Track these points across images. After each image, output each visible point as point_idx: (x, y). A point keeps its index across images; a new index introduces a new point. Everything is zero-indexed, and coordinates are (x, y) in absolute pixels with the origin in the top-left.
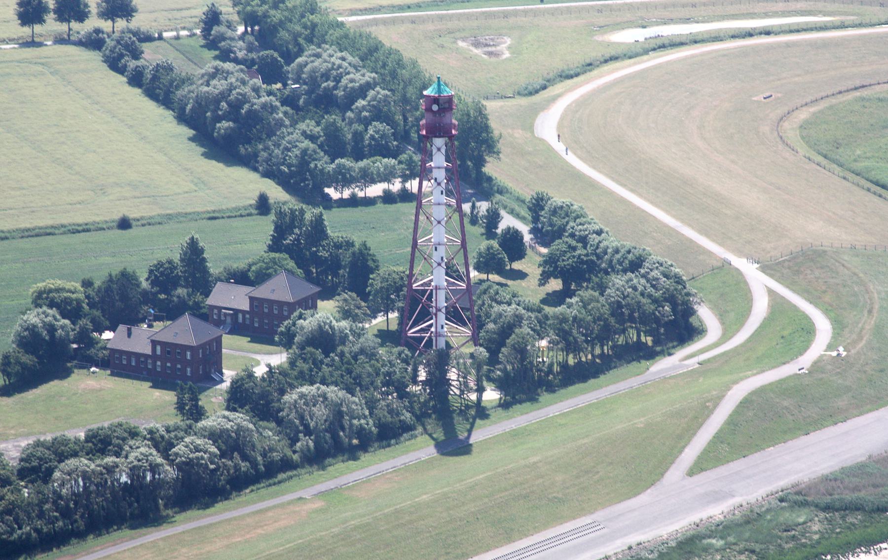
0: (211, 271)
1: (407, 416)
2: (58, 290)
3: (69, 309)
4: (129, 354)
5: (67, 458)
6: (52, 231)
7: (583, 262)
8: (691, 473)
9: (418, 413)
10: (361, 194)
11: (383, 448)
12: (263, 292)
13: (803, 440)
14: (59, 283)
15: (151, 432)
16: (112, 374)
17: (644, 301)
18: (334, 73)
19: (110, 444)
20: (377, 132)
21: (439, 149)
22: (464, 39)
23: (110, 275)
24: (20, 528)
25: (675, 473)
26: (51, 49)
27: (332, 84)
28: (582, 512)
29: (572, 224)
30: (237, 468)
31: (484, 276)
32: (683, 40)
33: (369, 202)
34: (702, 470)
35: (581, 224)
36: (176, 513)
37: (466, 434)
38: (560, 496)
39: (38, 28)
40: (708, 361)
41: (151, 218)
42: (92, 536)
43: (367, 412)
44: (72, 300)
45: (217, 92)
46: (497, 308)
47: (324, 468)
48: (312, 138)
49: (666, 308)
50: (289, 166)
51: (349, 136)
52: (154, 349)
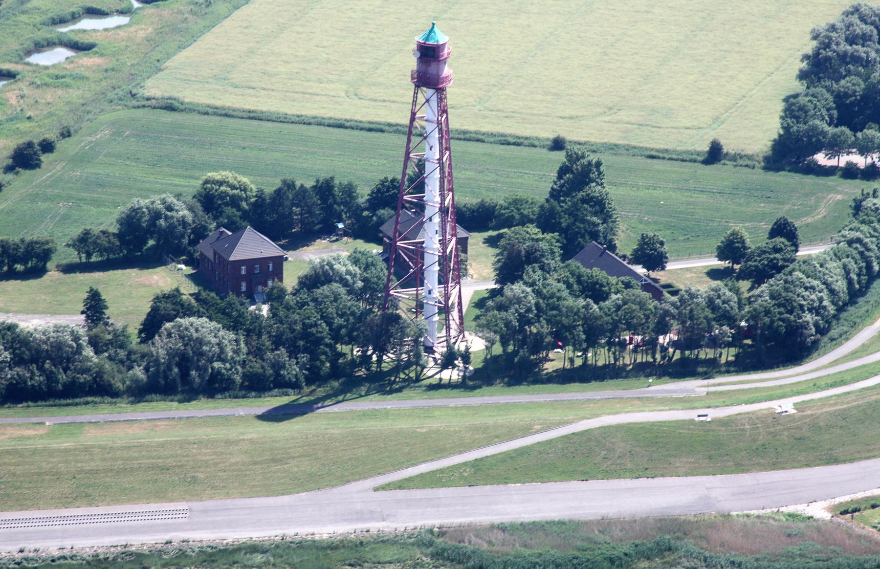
2: (221, 183)
38: (201, 476)
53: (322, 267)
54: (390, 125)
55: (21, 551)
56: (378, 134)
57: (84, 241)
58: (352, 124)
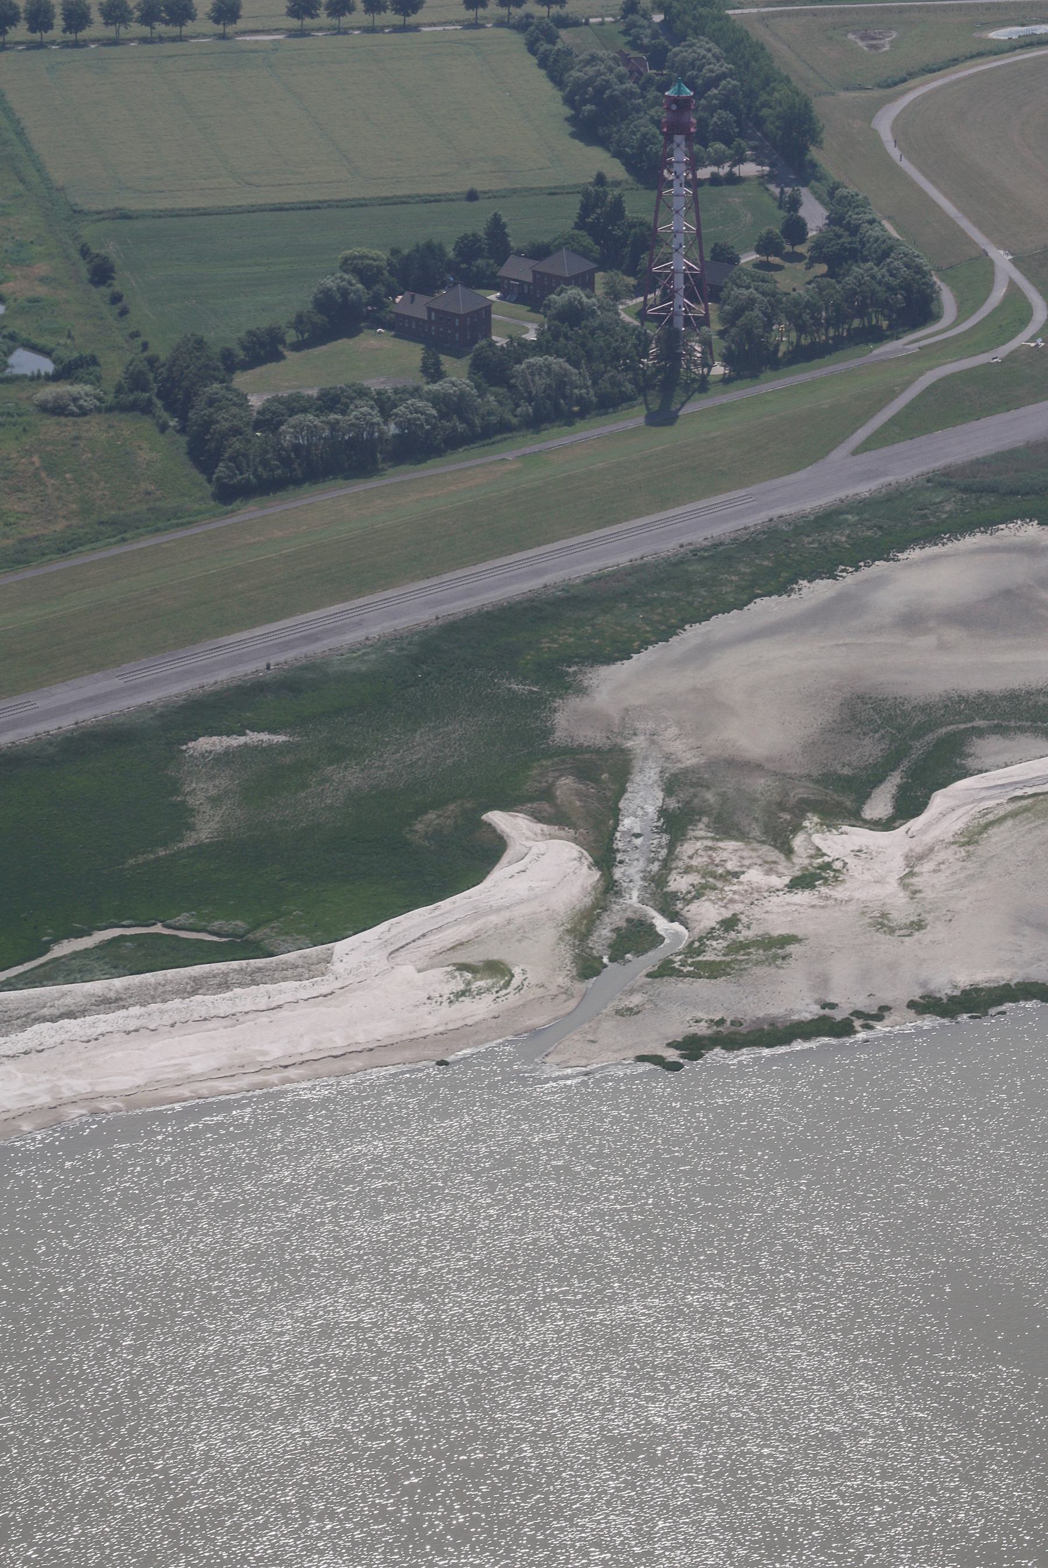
1: (629, 387)
2: (363, 257)
3: (367, 274)
4: (410, 318)
5: (296, 414)
6: (408, 200)
7: (846, 249)
8: (855, 453)
9: (642, 384)
11: (601, 415)
12: (545, 266)
14: (364, 250)
15: (379, 393)
16: (395, 336)
17: (878, 288)
18: (698, 63)
19: (338, 402)
20: (720, 119)
21: (678, 145)
22: (854, 32)
23: (417, 245)
24: (241, 474)
25: (839, 454)
26: (490, 31)
27: (695, 73)
29: (850, 213)
31: (764, 258)
34: (866, 450)
35: (857, 214)
36: (390, 467)
37: (678, 406)
39: (481, 12)
40: (925, 347)
41: (497, 191)
42: (307, 484)
43: (589, 383)
45: (586, 77)
46: (736, 291)
47: (538, 432)
48: (657, 123)
49: (899, 296)
50: (633, 148)
52: (429, 316)
54: (320, 202)
55: (681, 546)
56: (318, 211)
57: (299, 322)
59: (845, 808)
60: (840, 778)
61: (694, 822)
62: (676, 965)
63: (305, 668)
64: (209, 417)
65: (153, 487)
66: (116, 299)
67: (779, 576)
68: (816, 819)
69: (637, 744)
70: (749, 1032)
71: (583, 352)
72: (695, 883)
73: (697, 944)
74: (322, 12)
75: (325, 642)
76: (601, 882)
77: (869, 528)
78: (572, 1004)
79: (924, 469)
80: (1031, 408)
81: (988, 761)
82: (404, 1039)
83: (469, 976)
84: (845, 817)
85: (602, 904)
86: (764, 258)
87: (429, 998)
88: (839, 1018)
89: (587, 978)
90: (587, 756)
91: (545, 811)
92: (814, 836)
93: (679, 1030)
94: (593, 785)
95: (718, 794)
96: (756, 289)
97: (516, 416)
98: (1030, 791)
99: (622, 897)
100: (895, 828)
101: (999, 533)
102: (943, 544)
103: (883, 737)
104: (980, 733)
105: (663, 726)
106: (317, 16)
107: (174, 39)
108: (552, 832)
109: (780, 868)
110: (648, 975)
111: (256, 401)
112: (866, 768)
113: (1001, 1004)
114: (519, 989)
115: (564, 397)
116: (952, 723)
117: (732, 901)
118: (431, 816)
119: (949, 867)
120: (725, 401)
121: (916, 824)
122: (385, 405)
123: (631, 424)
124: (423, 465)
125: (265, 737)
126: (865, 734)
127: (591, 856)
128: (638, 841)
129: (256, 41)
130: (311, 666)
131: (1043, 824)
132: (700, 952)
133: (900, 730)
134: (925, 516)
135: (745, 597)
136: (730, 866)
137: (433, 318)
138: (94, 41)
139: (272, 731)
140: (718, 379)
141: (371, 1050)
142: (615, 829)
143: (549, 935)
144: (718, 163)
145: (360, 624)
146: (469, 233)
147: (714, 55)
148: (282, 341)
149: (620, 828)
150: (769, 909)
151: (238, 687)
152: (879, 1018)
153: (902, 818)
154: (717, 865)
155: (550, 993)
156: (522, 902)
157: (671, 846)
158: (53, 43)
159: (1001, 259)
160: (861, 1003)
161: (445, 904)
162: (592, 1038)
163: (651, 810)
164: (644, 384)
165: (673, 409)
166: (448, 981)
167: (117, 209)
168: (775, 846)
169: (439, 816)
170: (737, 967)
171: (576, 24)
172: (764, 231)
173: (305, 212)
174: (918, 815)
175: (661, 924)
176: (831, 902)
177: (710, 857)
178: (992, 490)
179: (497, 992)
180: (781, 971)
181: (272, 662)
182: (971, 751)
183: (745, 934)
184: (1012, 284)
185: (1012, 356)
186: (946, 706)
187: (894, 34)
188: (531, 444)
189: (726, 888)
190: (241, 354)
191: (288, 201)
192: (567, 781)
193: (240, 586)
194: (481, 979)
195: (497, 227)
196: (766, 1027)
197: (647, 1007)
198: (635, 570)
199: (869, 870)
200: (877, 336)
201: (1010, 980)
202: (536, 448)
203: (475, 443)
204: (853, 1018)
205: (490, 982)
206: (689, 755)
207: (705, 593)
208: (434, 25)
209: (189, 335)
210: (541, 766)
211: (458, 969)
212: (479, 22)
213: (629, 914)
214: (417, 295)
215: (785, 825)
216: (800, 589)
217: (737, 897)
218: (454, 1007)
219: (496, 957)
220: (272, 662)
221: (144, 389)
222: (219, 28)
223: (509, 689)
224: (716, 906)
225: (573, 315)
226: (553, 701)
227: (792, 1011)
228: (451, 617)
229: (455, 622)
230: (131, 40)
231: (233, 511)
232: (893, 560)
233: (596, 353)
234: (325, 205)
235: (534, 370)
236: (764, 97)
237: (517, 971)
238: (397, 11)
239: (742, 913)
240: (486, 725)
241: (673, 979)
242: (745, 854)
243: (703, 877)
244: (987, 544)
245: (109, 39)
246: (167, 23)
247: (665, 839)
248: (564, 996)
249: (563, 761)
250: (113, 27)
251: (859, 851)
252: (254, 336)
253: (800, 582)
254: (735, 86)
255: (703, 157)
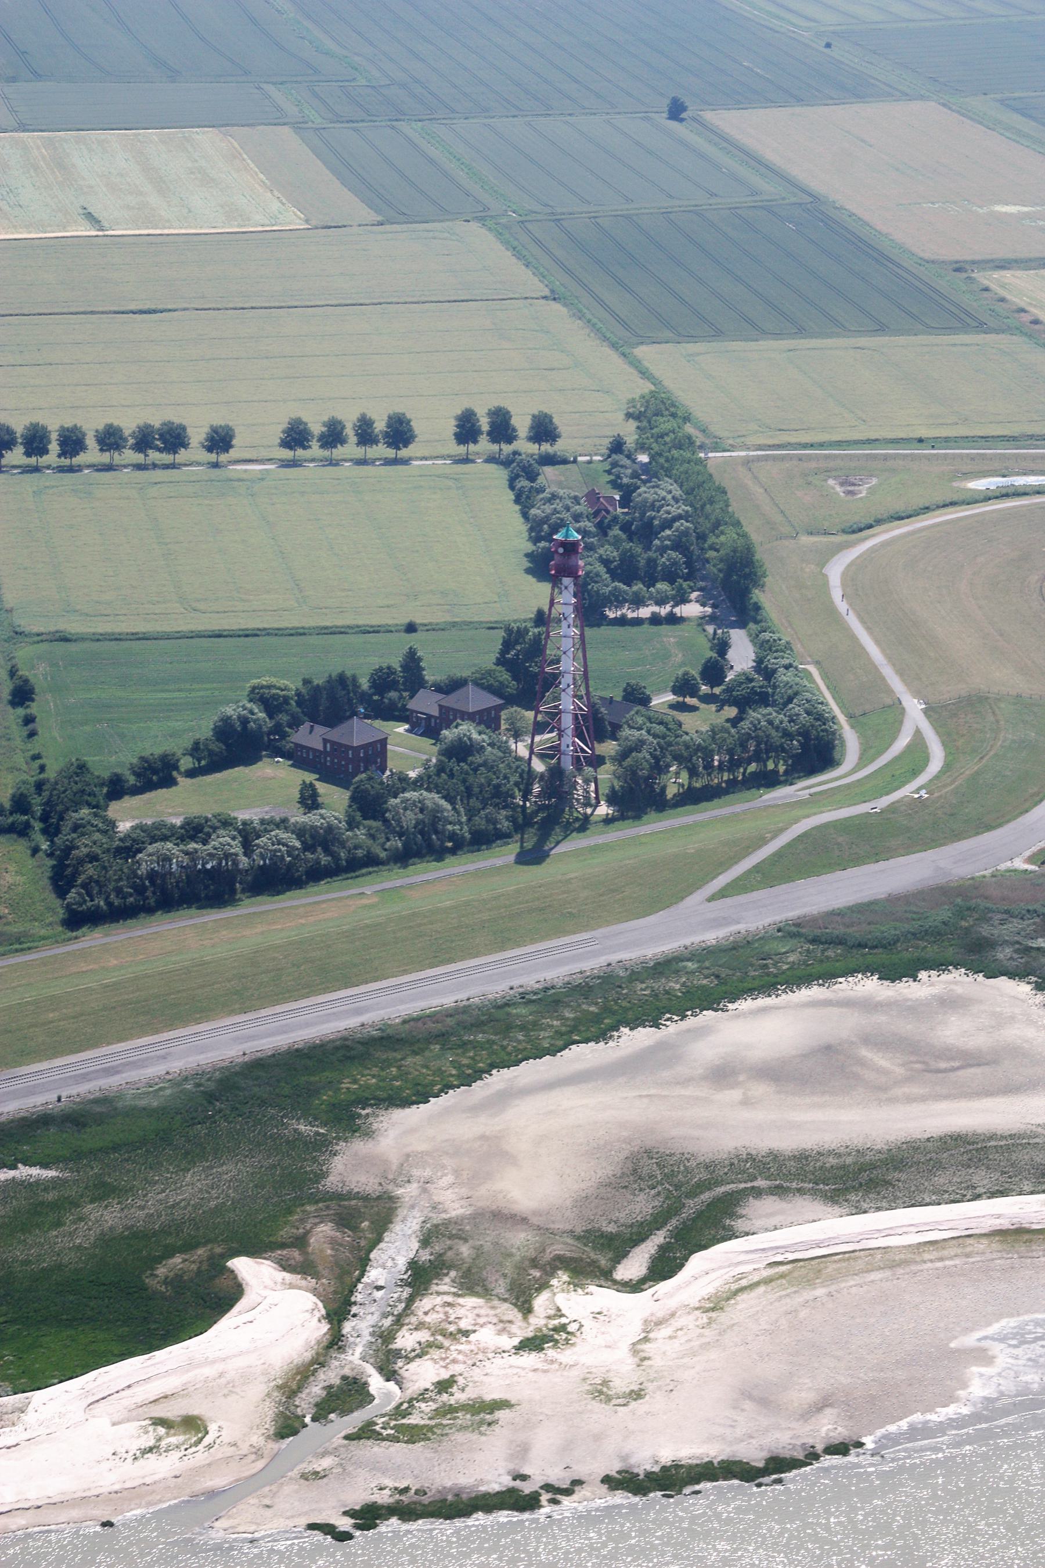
0: (427, 678)
2: (269, 687)
3: (271, 703)
4: (308, 749)
5: (156, 842)
6: (258, 632)
8: (711, 899)
10: (631, 615)
11: (473, 852)
12: (451, 701)
13: (839, 874)
14: (273, 680)
15: (244, 823)
16: (292, 766)
17: (774, 733)
18: (657, 504)
19: (201, 831)
21: (566, 588)
22: (835, 478)
24: (92, 900)
26: (480, 466)
28: (586, 928)
30: (318, 862)
31: (681, 699)
32: (1028, 490)
33: (638, 622)
34: (724, 897)
35: (775, 658)
36: (248, 897)
38: (574, 911)
39: (472, 447)
40: (815, 794)
41: (437, 624)
42: (159, 913)
43: (464, 819)
44: (280, 696)
49: (795, 742)
51: (642, 563)
52: (325, 747)
53: (460, 739)
54: (259, 630)
55: (511, 988)
57: (195, 750)
58: (231, 633)
59: (599, 1267)
60: (603, 1235)
61: (439, 1276)
62: (377, 1428)
63: (96, 1101)
64: (71, 842)
65: (6, 911)
66: (29, 720)
67: (602, 1023)
68: (565, 1278)
69: (407, 1192)
70: (430, 1503)
71: (463, 788)
72: (423, 1340)
73: (405, 1405)
74: (315, 444)
75: (124, 1075)
76: (328, 1336)
77: (706, 977)
78: (260, 1464)
79: (778, 918)
80: (901, 860)
81: (758, 1223)
82: (76, 1496)
83: (161, 1431)
84: (596, 1276)
85: (322, 1359)
86: (681, 699)
87: (114, 1454)
88: (527, 1491)
89: (283, 1438)
90: (353, 1202)
91: (294, 1259)
92: (558, 1295)
93: (359, 1496)
94: (350, 1233)
95: (474, 1248)
96: (648, 732)
97: (386, 850)
98: (791, 1257)
99: (344, 1352)
100: (643, 1290)
101: (838, 985)
102: (777, 996)
103: (659, 1193)
104: (758, 1193)
105: (439, 1174)
106: (310, 447)
107: (166, 467)
108: (294, 1281)
109: (514, 1328)
110: (347, 1437)
111: (124, 826)
112: (632, 1226)
113: (698, 1482)
114: (209, 1447)
115: (436, 832)
116: (733, 1183)
117: (454, 1361)
118: (177, 1260)
119: (686, 1334)
120: (600, 841)
121: (664, 1287)
122: (248, 835)
123: (499, 862)
124: (281, 897)
125: (35, 1172)
126: (641, 1190)
127: (325, 1307)
128: (378, 1295)
129: (246, 471)
130: (106, 1102)
131: (795, 1292)
132: (405, 1414)
133: (677, 1187)
134: (766, 966)
135: (560, 1043)
136: (464, 1325)
137: (328, 749)
138: (89, 466)
139: (45, 1166)
140: (600, 819)
141: (39, 1507)
142: (359, 1280)
143: (258, 1390)
144: (660, 603)
145: (164, 1057)
146: (385, 665)
147: (673, 498)
148: (176, 768)
149: (365, 1280)
150: (489, 1371)
151: (23, 1119)
152: (568, 1492)
153: (654, 1281)
154: (450, 1323)
155: (240, 1452)
156: (241, 1353)
157: (410, 1301)
158: (48, 467)
159: (914, 707)
160: (557, 1476)
161: (159, 1355)
162: (268, 1503)
163: (402, 1262)
164: (522, 823)
165: (546, 848)
166: (139, 1436)
167: (57, 632)
168: (515, 1305)
169: (185, 1260)
170: (439, 1432)
171: (564, 462)
172: (680, 672)
173: (242, 639)
174: (670, 1277)
175: (376, 1383)
176: (555, 1366)
177: (446, 1313)
178: (839, 941)
179: (186, 1449)
180: (483, 1438)
181: (64, 1095)
182: (744, 1212)
183: (458, 1397)
184: (918, 733)
185: (892, 808)
186: (732, 1164)
187: (874, 481)
188: (394, 879)
189: (452, 1348)
190: (132, 780)
191: (227, 627)
192: (324, 1228)
193: (51, 1015)
194: (174, 1435)
195: (412, 662)
196: (450, 1497)
197: (334, 1471)
198: (459, 1011)
199: (603, 1333)
200: (770, 780)
201: (715, 1457)
202: (398, 883)
203: (337, 875)
204: (542, 1492)
205: (181, 1438)
206: (456, 1205)
207: (521, 1038)
208: (425, 458)
209: (74, 760)
210: (304, 1211)
211: (154, 1424)
212: (470, 457)
213: (347, 1371)
214: (316, 726)
215: (533, 1282)
216: (619, 1037)
217: (460, 1357)
218: (137, 1463)
219: (196, 1413)
220: (64, 1095)
221: (25, 812)
222: (213, 457)
223: (296, 1130)
224: (437, 1366)
225: (461, 751)
226: (337, 1144)
227: (482, 1481)
228: (259, 1054)
229: (261, 1059)
230: (125, 466)
231: (76, 938)
232: (722, 1010)
233: (476, 790)
234: (264, 633)
235: (407, 805)
236: (712, 539)
237: (212, 1428)
238: (389, 445)
239: (461, 1375)
240: (262, 1167)
241: (369, 1443)
242: (482, 1312)
243: (433, 1335)
244: (822, 997)
245: (105, 465)
246: (160, 450)
247: (408, 1291)
248: (253, 1457)
249: (328, 1207)
250: (108, 453)
251: (599, 1313)
252: (146, 762)
253: (622, 1029)
254: (688, 528)
255: (644, 597)
